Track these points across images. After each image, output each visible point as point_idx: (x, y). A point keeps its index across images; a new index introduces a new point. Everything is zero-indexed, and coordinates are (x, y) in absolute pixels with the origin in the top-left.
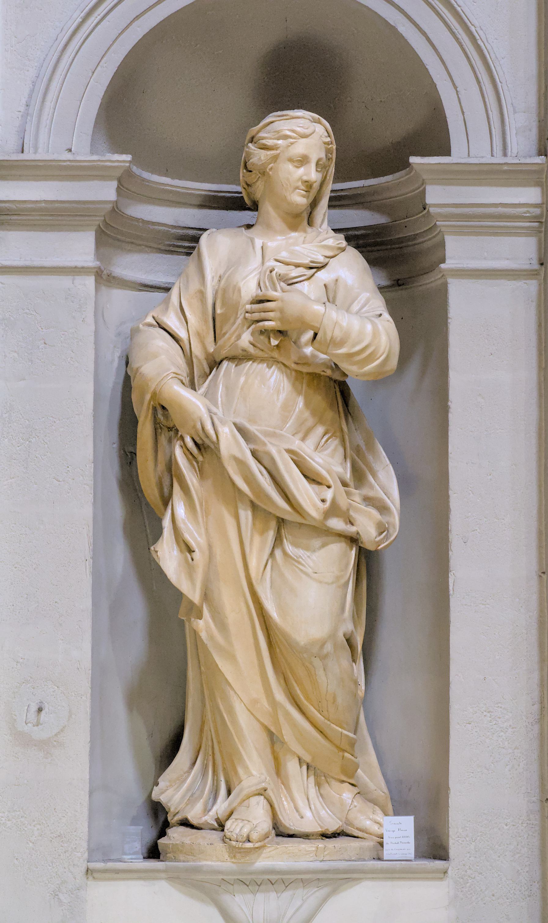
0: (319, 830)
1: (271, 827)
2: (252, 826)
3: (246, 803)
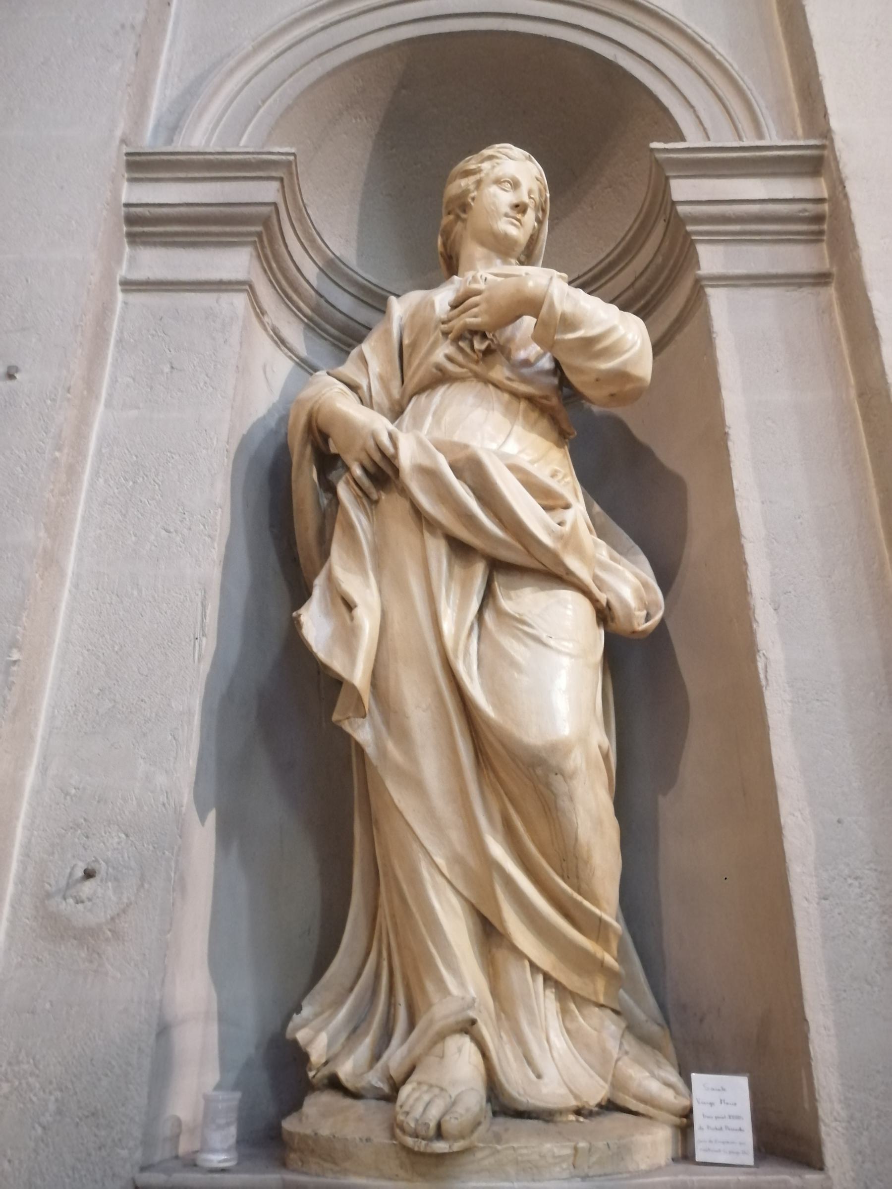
0: (573, 1103)
1: (484, 1100)
2: (448, 1099)
3: (438, 1049)
